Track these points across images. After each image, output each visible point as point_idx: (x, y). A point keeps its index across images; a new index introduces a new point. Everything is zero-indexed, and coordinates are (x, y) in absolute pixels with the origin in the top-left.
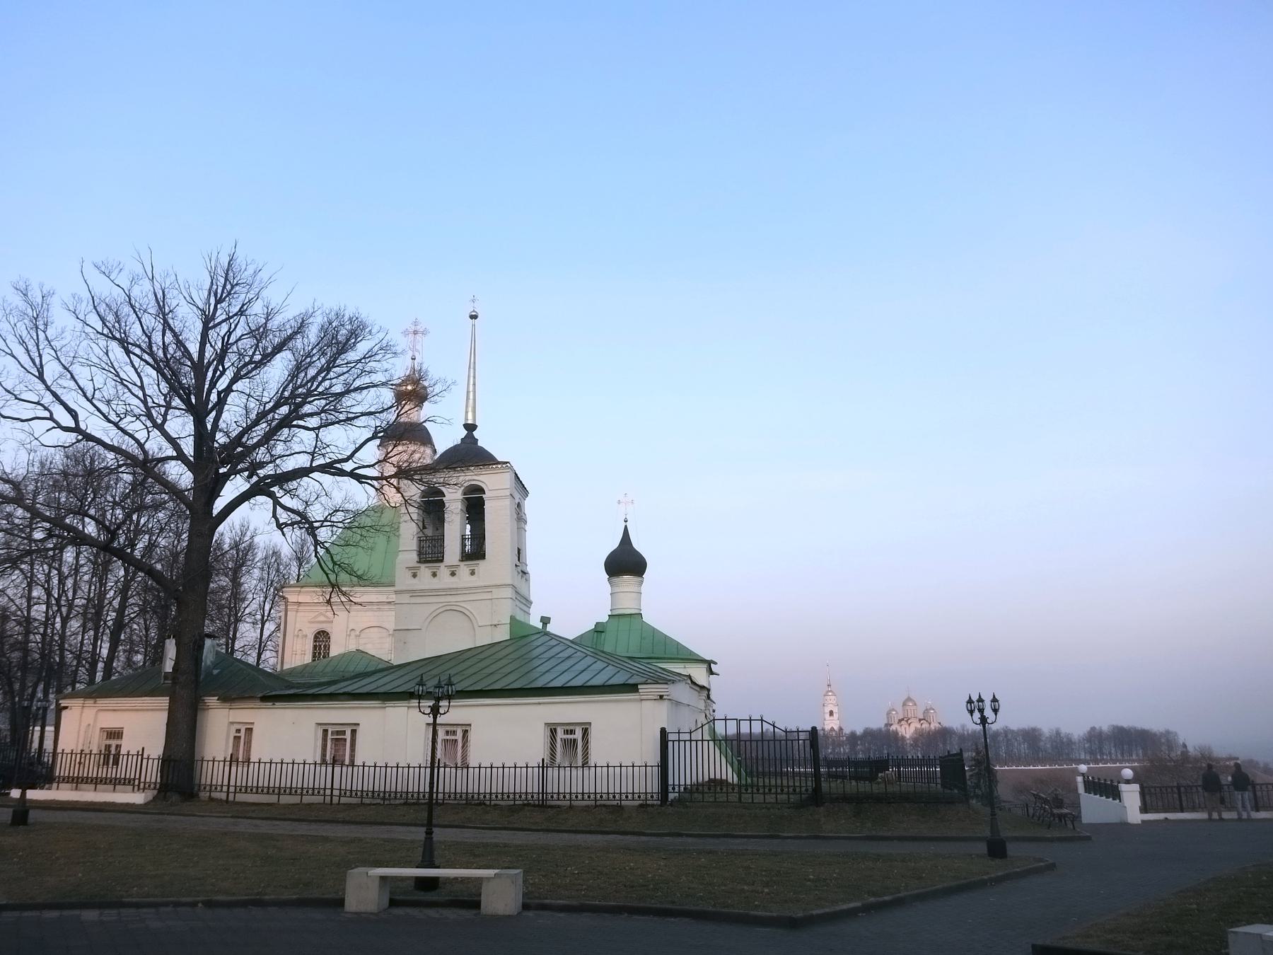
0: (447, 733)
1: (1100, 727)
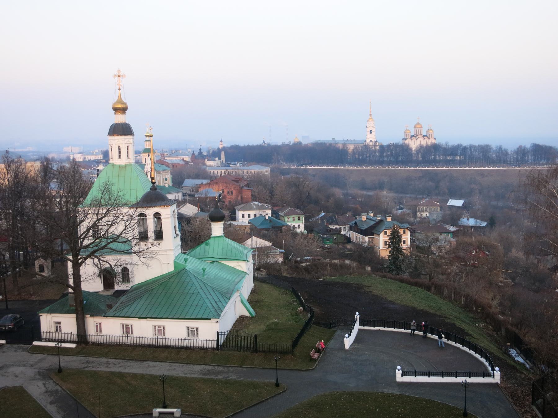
0: (159, 327)
1: (525, 146)
